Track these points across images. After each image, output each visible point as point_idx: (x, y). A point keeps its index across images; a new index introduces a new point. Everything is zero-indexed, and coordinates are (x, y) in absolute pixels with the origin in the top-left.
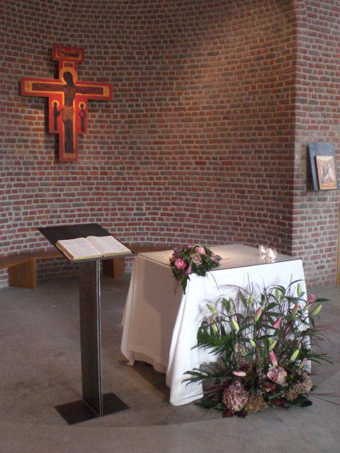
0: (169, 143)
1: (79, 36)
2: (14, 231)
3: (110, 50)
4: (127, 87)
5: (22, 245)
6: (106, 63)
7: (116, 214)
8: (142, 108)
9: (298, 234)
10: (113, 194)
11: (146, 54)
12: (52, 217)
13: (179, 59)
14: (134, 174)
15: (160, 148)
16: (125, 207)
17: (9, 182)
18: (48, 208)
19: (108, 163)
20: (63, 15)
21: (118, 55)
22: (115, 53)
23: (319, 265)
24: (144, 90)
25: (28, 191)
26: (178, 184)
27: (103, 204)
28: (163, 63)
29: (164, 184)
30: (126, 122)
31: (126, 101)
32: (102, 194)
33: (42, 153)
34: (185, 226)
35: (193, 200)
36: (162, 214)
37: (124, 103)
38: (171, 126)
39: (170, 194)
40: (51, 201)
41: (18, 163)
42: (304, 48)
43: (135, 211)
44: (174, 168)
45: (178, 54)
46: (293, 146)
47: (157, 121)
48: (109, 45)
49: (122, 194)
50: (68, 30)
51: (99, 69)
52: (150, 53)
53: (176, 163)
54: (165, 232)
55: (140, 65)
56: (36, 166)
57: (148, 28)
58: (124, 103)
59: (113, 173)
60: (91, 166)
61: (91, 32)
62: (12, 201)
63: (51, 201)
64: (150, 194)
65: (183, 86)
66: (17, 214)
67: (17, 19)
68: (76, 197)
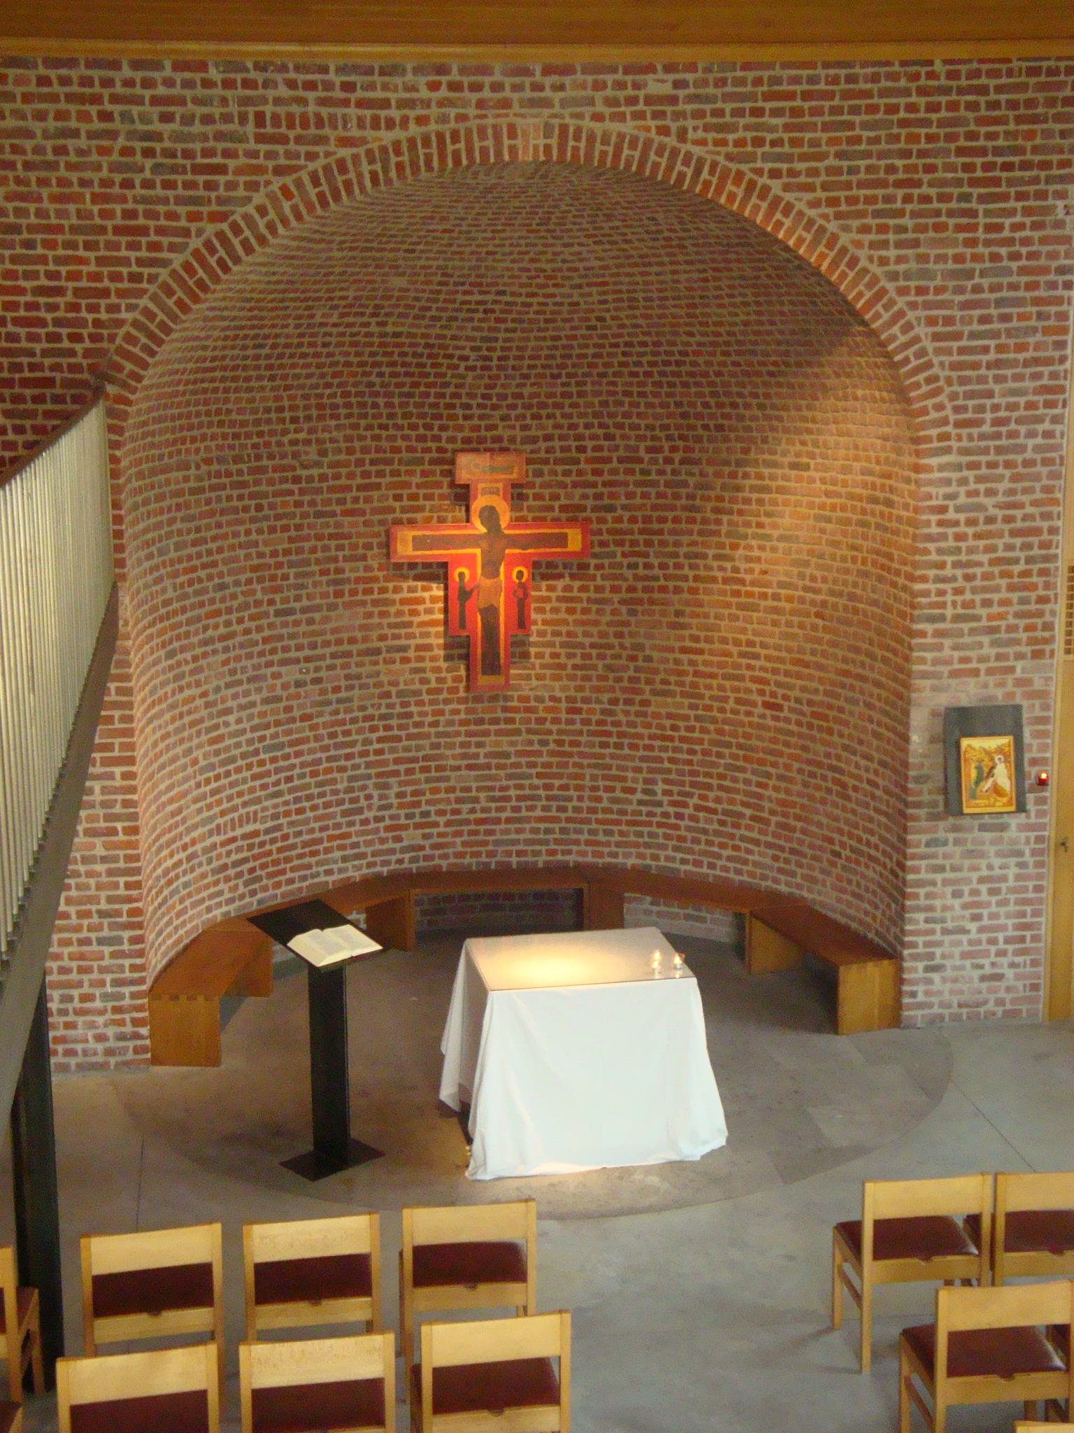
0: (711, 653)
2: (377, 830)
3: (590, 444)
4: (625, 525)
5: (394, 858)
6: (580, 473)
7: (599, 799)
8: (656, 572)
9: (922, 902)
11: (667, 453)
12: (458, 800)
13: (733, 468)
14: (638, 714)
15: (691, 663)
16: (618, 785)
17: (368, 735)
18: (452, 783)
19: (580, 689)
20: (481, 377)
21: (605, 454)
23: (988, 970)
24: (660, 532)
26: (729, 745)
27: (570, 776)
28: (702, 474)
29: (701, 741)
30: (622, 602)
31: (624, 555)
32: (570, 755)
33: (438, 670)
34: (742, 838)
35: (759, 785)
36: (698, 808)
37: (619, 559)
38: (717, 617)
39: (713, 765)
40: (459, 768)
42: (940, 502)
44: (722, 710)
45: (733, 458)
47: (687, 603)
48: (587, 432)
49: (613, 756)
50: (494, 407)
52: (674, 449)
53: (725, 699)
54: (703, 847)
55: (654, 477)
56: (425, 697)
57: (669, 395)
58: (619, 559)
59: (591, 711)
60: (546, 695)
61: (544, 406)
62: (373, 771)
63: (459, 768)
64: (671, 760)
65: (742, 530)
66: (381, 797)
67: (381, 401)
68: (513, 760)
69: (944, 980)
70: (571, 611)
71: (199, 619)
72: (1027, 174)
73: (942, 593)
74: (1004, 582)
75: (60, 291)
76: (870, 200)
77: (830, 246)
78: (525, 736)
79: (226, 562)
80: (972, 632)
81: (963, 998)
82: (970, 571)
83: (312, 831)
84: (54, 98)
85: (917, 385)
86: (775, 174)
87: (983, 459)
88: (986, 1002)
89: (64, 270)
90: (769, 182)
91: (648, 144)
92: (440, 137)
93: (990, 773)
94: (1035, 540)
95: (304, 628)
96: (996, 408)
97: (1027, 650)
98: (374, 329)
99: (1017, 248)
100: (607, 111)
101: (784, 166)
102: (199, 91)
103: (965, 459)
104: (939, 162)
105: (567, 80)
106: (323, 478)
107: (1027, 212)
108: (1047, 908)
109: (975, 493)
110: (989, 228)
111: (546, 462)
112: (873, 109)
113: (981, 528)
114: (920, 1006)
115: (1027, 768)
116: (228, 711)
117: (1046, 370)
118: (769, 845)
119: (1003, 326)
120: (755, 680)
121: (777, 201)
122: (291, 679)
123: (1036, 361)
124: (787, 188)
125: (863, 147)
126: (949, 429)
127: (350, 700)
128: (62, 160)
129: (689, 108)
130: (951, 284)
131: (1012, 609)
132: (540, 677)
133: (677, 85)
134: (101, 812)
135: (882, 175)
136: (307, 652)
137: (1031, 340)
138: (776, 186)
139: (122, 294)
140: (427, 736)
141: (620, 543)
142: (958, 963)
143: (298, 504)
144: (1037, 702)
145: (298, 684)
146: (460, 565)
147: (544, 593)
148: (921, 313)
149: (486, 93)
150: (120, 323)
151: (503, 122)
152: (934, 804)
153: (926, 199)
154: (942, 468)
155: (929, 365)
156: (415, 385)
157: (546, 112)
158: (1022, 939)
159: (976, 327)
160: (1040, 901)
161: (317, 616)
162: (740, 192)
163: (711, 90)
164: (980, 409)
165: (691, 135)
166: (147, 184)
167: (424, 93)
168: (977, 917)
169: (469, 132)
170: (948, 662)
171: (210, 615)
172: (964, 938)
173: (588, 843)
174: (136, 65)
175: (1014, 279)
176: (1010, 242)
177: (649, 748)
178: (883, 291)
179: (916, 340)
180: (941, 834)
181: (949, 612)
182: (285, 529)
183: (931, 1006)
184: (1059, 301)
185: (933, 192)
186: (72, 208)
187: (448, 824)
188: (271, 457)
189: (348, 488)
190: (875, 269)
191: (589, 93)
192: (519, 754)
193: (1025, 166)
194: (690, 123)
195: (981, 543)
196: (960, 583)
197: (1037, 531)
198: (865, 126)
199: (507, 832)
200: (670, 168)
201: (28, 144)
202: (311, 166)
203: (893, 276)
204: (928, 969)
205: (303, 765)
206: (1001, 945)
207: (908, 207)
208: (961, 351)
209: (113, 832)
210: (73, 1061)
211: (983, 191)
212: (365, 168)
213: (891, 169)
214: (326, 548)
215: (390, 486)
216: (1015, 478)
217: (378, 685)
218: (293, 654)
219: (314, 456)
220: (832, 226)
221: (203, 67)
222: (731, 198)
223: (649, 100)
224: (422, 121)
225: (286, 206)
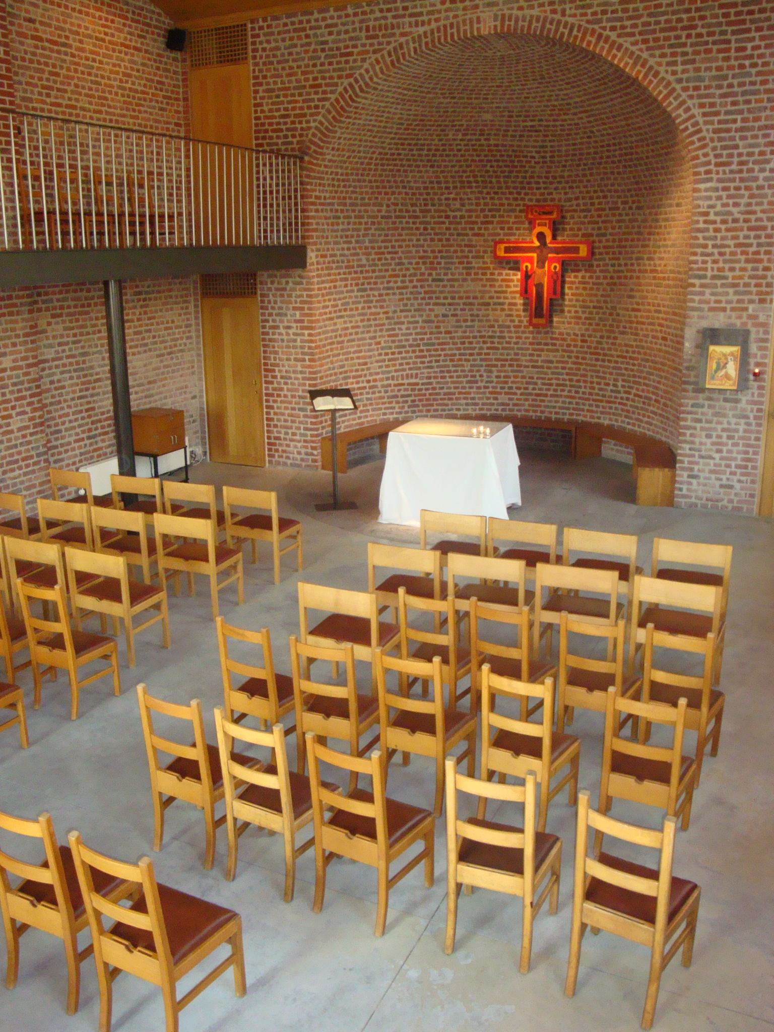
1: (564, 188)
2: (484, 393)
3: (596, 201)
9: (688, 438)
12: (527, 383)
19: (587, 330)
23: (724, 482)
25: (502, 354)
33: (519, 316)
40: (527, 367)
43: (611, 387)
49: (601, 366)
50: (551, 183)
51: (583, 223)
59: (592, 342)
62: (484, 363)
63: (527, 367)
67: (494, 180)
69: (699, 484)
70: (585, 289)
72: (763, 16)
73: (704, 262)
74: (743, 258)
76: (666, 39)
77: (643, 66)
78: (561, 353)
80: (723, 285)
81: (710, 496)
82: (723, 250)
83: (449, 388)
85: (693, 143)
86: (613, 29)
87: (732, 185)
88: (722, 500)
89: (290, 106)
90: (610, 33)
92: (445, 26)
93: (725, 366)
94: (762, 233)
96: (740, 155)
97: (756, 298)
98: (483, 142)
99: (755, 60)
101: (618, 24)
103: (720, 185)
104: (708, 13)
106: (462, 217)
109: (726, 205)
110: (738, 50)
111: (575, 211)
113: (730, 225)
114: (684, 496)
116: (403, 323)
119: (745, 107)
122: (440, 313)
124: (619, 36)
125: (663, 9)
126: (712, 167)
127: (473, 326)
131: (747, 274)
134: (299, 350)
135: (674, 24)
136: (449, 301)
137: (763, 114)
138: (613, 35)
139: (312, 115)
140: (513, 349)
142: (708, 475)
143: (447, 229)
144: (761, 330)
145: (444, 316)
146: (524, 262)
148: (696, 101)
150: (309, 128)
151: (474, 16)
153: (699, 35)
154: (706, 190)
155: (700, 131)
156: (510, 172)
157: (495, 9)
158: (746, 467)
159: (729, 108)
161: (456, 284)
162: (593, 40)
164: (731, 156)
165: (568, 12)
169: (458, 23)
170: (708, 302)
172: (712, 462)
173: (588, 411)
175: (753, 79)
176: (751, 57)
177: (616, 362)
178: (674, 90)
179: (693, 116)
180: (701, 401)
181: (709, 273)
182: (440, 240)
183: (690, 497)
185: (704, 31)
187: (522, 394)
188: (433, 205)
192: (558, 362)
195: (730, 234)
196: (717, 257)
199: (550, 401)
200: (556, 31)
201: (279, 53)
202: (389, 48)
203: (679, 81)
204: (689, 476)
205: (445, 355)
206: (733, 469)
207: (689, 41)
208: (719, 122)
210: (289, 462)
211: (735, 28)
212: (412, 45)
215: (498, 223)
216: (751, 196)
217: (488, 321)
219: (458, 206)
220: (645, 55)
224: (437, 20)
225: (377, 68)
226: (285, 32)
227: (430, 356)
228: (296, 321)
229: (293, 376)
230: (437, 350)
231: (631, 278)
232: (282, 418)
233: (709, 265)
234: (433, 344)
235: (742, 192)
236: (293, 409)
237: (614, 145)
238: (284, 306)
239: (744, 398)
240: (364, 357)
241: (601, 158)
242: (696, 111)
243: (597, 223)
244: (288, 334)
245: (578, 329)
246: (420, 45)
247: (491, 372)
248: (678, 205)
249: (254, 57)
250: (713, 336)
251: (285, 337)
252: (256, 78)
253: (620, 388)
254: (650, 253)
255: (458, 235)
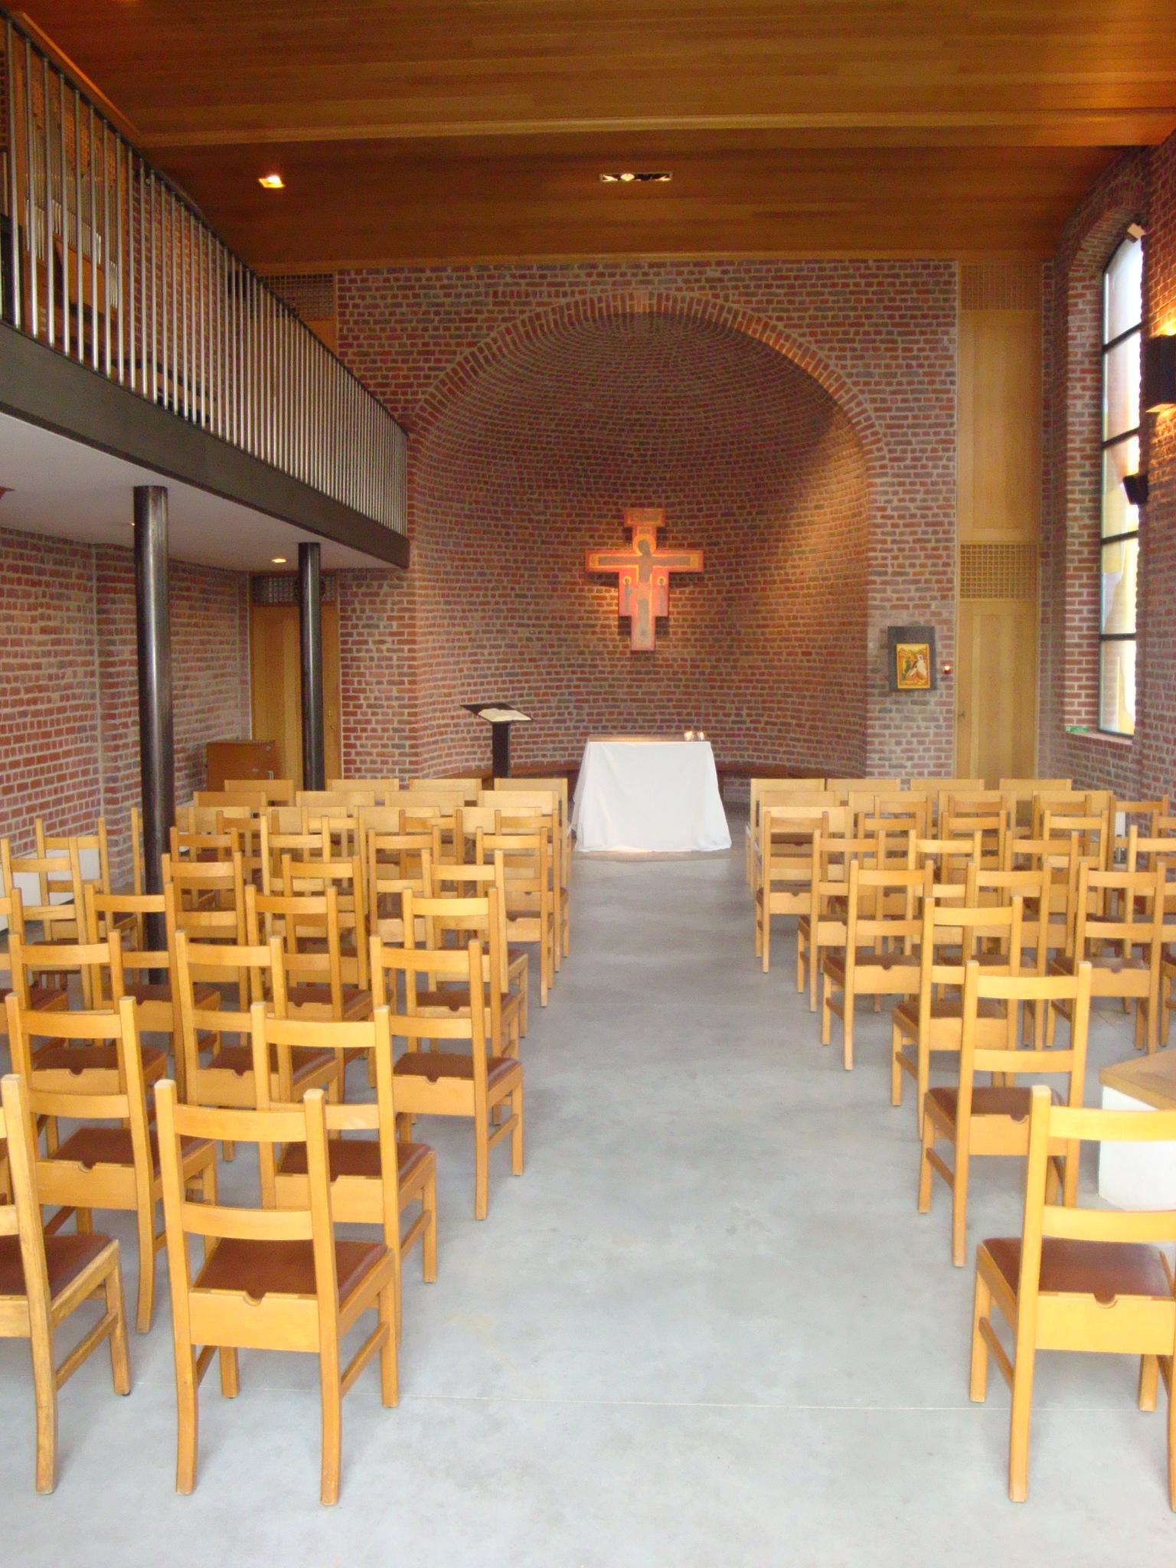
9: (877, 747)
10: (705, 694)
12: (626, 721)
19: (698, 653)
22: (711, 509)
33: (614, 640)
36: (767, 723)
40: (623, 701)
41: (582, 653)
43: (733, 718)
46: (864, 632)
50: (649, 485)
62: (573, 698)
64: (752, 695)
67: (582, 479)
71: (466, 589)
73: (884, 558)
74: (922, 553)
75: (387, 385)
79: (486, 561)
80: (904, 582)
84: (391, 288)
85: (866, 437)
86: (779, 319)
87: (908, 480)
89: (390, 374)
91: (707, 303)
95: (532, 607)
96: (913, 451)
100: (684, 286)
101: (785, 315)
102: (465, 282)
103: (896, 480)
104: (874, 313)
105: (662, 270)
107: (926, 342)
108: (954, 754)
109: (902, 500)
110: (905, 350)
111: (680, 517)
112: (834, 285)
113: (908, 521)
115: (938, 666)
116: (484, 647)
117: (943, 430)
118: (805, 740)
119: (916, 405)
120: (797, 639)
121: (780, 334)
123: (937, 425)
124: (786, 326)
128: (393, 319)
129: (730, 284)
130: (884, 380)
132: (675, 647)
133: (725, 272)
134: (396, 671)
138: (780, 325)
139: (419, 385)
141: (722, 564)
143: (532, 535)
147: (678, 596)
148: (867, 396)
149: (618, 278)
150: (416, 401)
151: (627, 293)
152: (883, 686)
153: (867, 333)
154: (882, 485)
155: (872, 426)
156: (603, 471)
157: (650, 287)
159: (900, 405)
160: (951, 750)
161: (541, 601)
162: (760, 328)
163: (742, 275)
164: (904, 451)
166: (436, 329)
167: (583, 278)
168: (911, 759)
170: (889, 600)
171: (474, 589)
174: (433, 270)
176: (917, 358)
178: (844, 383)
180: (888, 706)
181: (890, 570)
182: (523, 548)
184: (948, 391)
186: (397, 342)
188: (516, 506)
189: (562, 529)
190: (839, 370)
191: (674, 277)
192: (663, 693)
193: (924, 317)
194: (731, 292)
195: (908, 530)
196: (896, 553)
197: (941, 524)
198: (830, 294)
200: (719, 316)
203: (850, 375)
209: (402, 683)
212: (551, 317)
213: (847, 317)
214: (547, 563)
216: (927, 492)
217: (578, 646)
218: (526, 621)
219: (542, 509)
221: (467, 269)
222: (755, 331)
223: (708, 280)
224: (581, 292)
225: (508, 338)
226: (385, 288)
227: (513, 689)
228: (392, 634)
229: (385, 703)
230: (519, 682)
231: (755, 590)
232: (368, 759)
233: (889, 562)
234: (517, 674)
235: (918, 487)
236: (384, 746)
237: (733, 443)
238: (376, 615)
239: (933, 699)
240: (449, 687)
241: (714, 458)
242: (867, 406)
243: (706, 530)
244: (379, 650)
245: (688, 653)
246: (562, 317)
247: (581, 708)
248: (817, 507)
249: (343, 314)
250: (898, 635)
251: (375, 655)
252: (342, 337)
253: (745, 718)
254: (779, 561)
255: (543, 542)
